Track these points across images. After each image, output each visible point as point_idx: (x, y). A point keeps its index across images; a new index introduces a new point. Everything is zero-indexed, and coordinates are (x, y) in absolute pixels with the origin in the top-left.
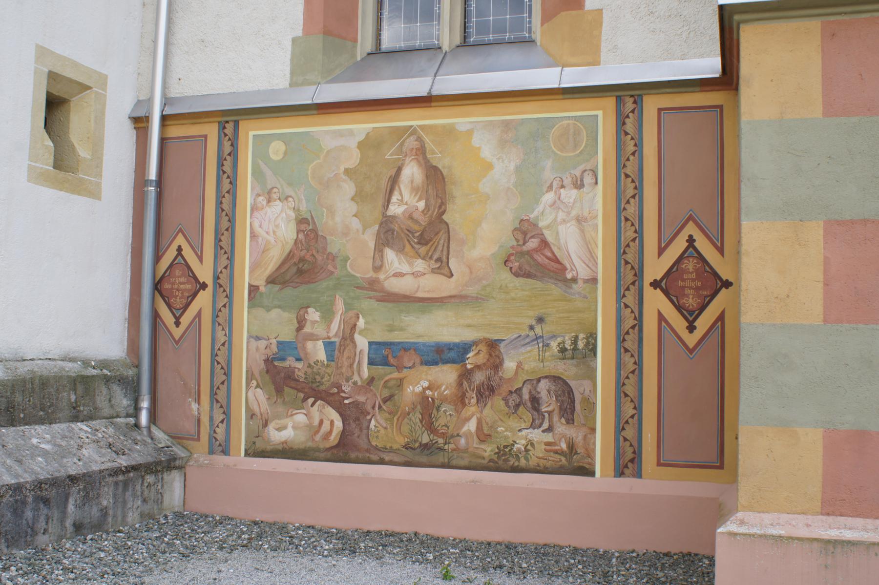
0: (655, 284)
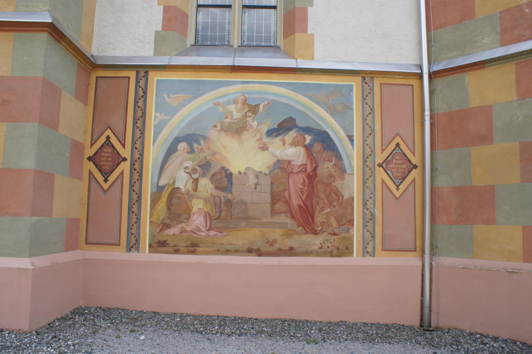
0: (125, 159)
